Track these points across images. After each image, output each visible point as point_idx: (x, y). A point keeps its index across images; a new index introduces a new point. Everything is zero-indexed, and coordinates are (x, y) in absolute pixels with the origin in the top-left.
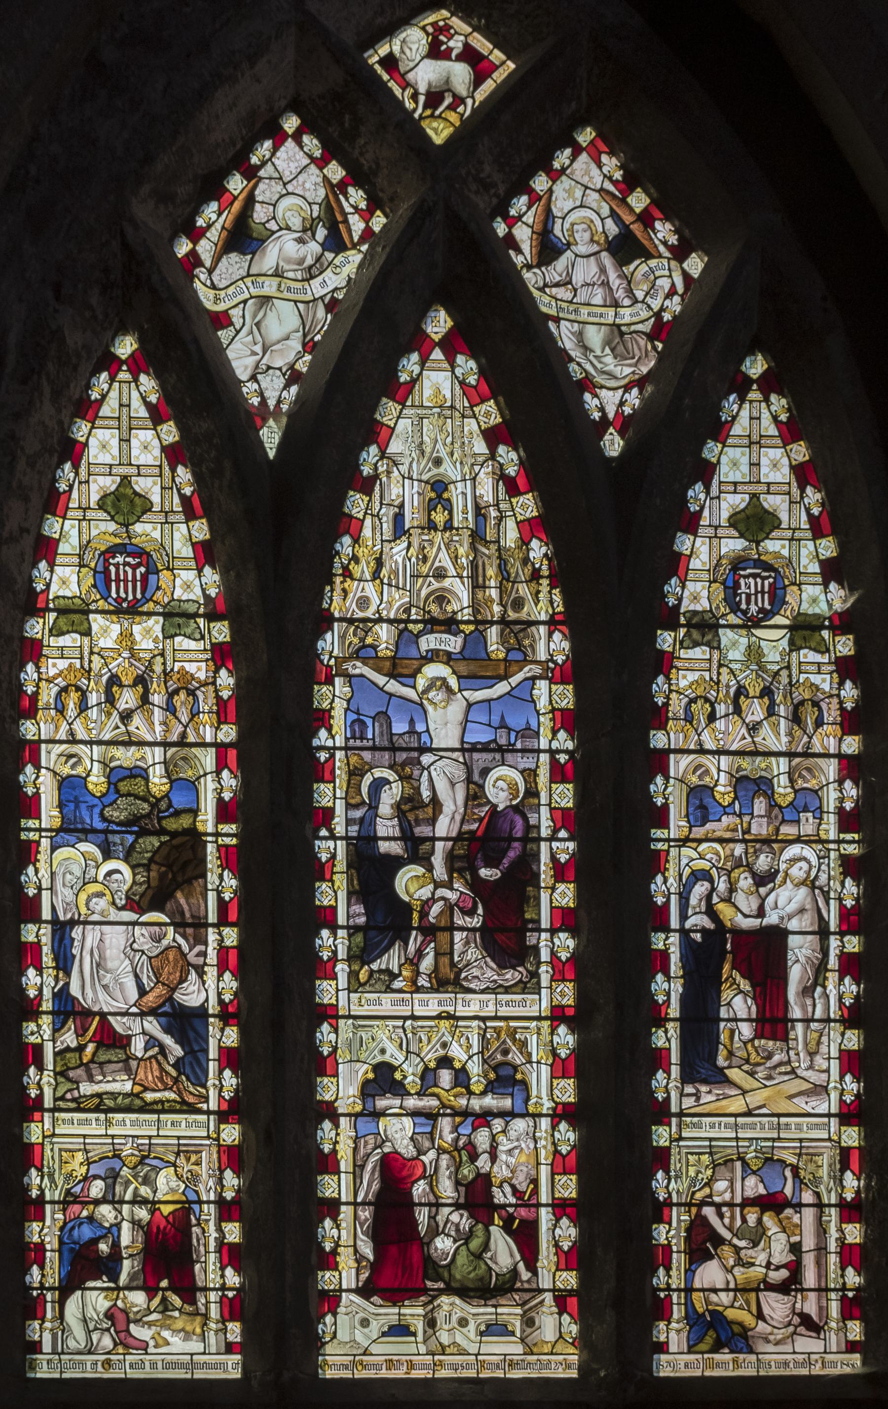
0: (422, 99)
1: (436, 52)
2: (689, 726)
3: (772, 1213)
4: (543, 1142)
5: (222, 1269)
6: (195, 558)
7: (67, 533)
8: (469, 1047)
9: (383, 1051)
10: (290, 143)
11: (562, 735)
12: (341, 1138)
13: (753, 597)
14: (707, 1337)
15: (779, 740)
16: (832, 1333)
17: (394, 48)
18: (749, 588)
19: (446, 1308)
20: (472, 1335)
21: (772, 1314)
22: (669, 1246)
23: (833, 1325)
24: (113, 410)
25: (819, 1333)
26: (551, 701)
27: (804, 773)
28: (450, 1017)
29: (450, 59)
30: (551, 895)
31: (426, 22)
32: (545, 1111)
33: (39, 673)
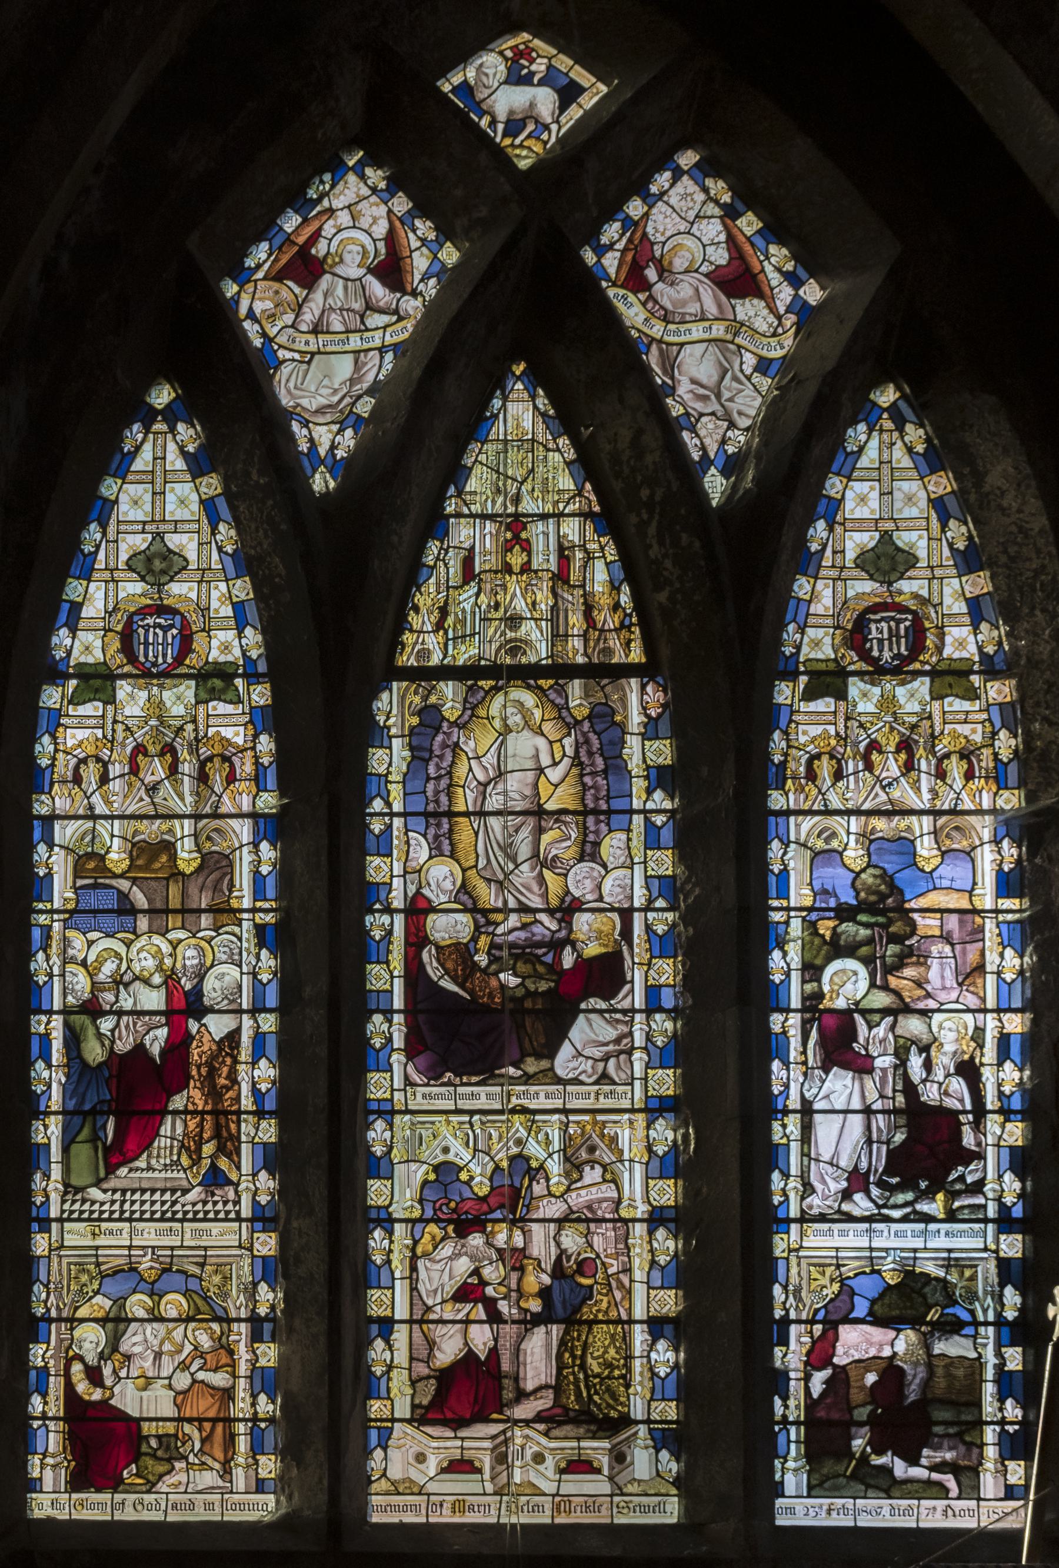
0: (500, 127)
1: (517, 78)
2: (77, 789)
4: (638, 1250)
5: (254, 1396)
6: (969, 613)
7: (820, 593)
8: (548, 1142)
9: (446, 1150)
10: (352, 178)
11: (658, 795)
12: (395, 1247)
13: (886, 643)
15: (182, 799)
17: (469, 75)
18: (881, 632)
19: (518, 1441)
20: (550, 1473)
22: (46, 1368)
23: (241, 1460)
24: (146, 464)
26: (644, 761)
27: (214, 835)
28: (524, 1110)
29: (531, 84)
30: (647, 972)
31: (504, 47)
32: (639, 1216)
33: (56, 744)
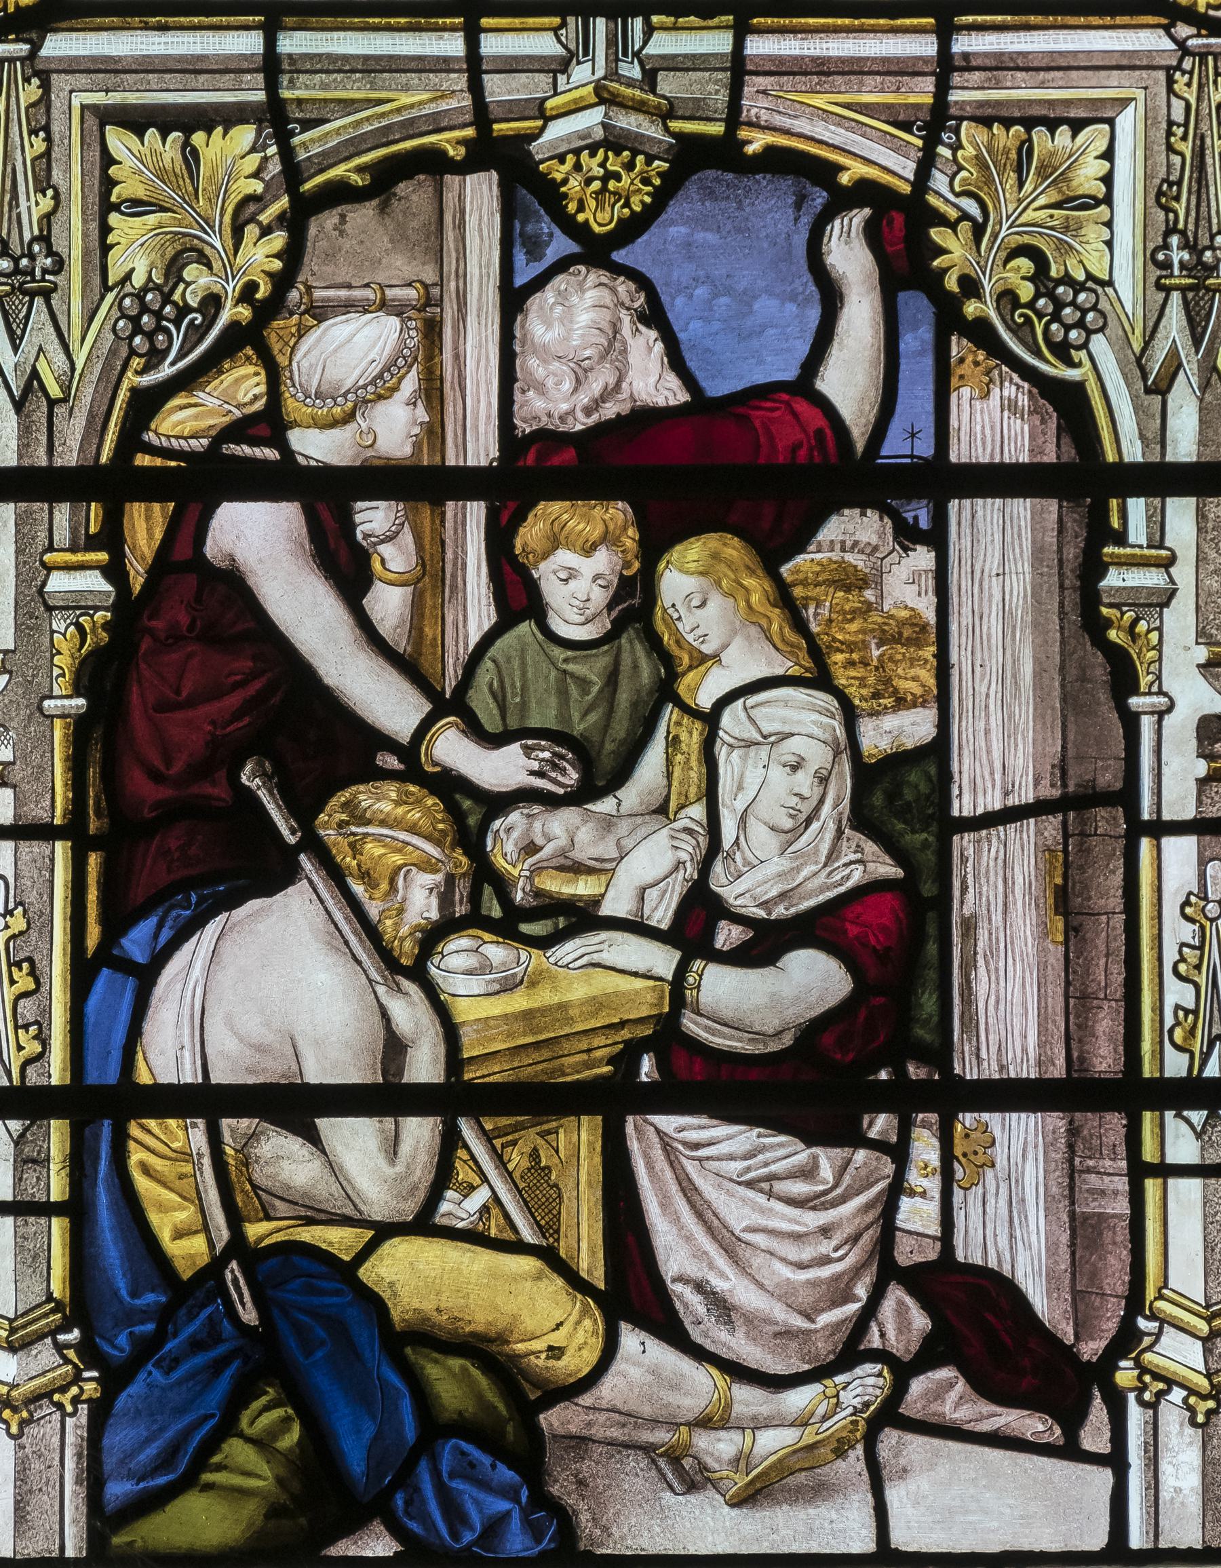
3: (733, 548)
14: (237, 1450)
16: (1172, 1415)
21: (727, 1282)
25: (1072, 1420)
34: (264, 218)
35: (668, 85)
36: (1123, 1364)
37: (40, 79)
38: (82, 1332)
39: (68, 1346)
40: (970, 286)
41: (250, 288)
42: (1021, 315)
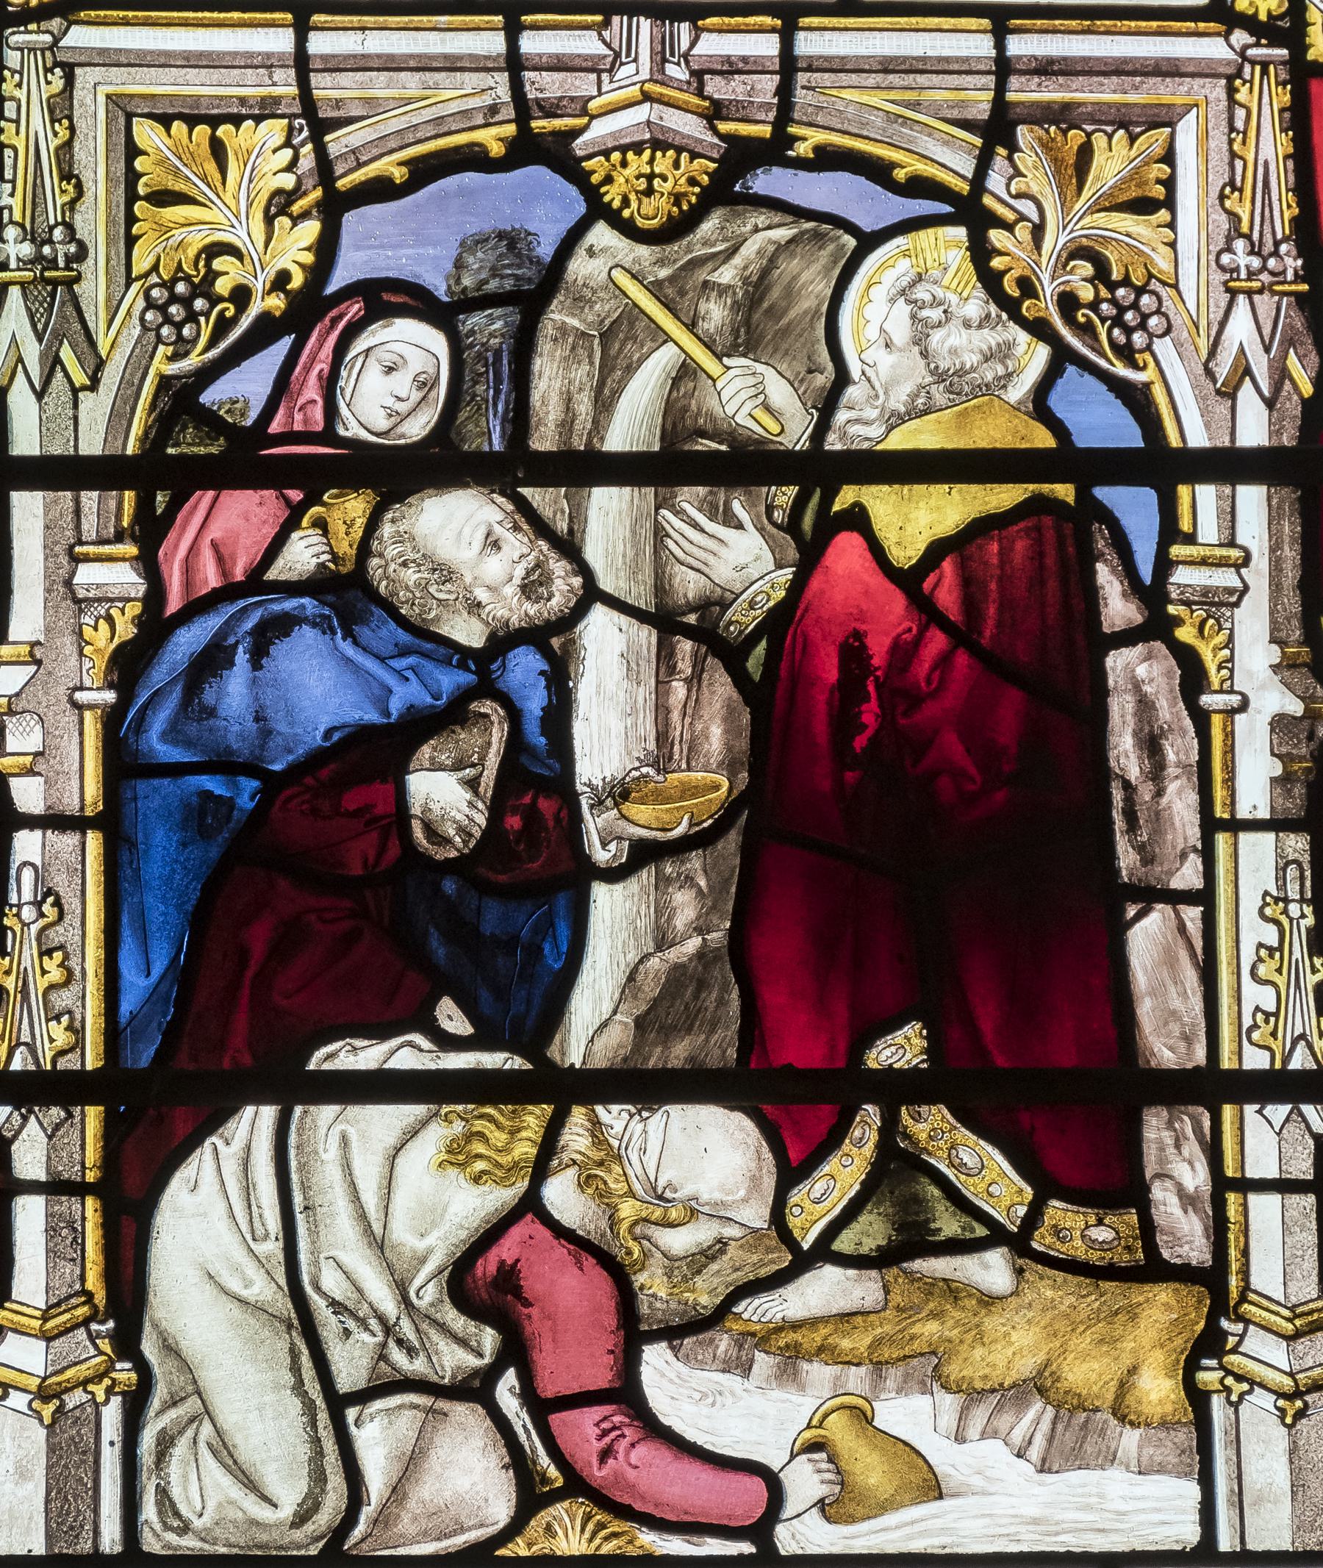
34: (296, 208)
35: (715, 87)
36: (1206, 1362)
37: (63, 70)
38: (116, 1322)
39: (99, 1335)
40: (1028, 288)
41: (282, 280)
42: (1083, 315)
